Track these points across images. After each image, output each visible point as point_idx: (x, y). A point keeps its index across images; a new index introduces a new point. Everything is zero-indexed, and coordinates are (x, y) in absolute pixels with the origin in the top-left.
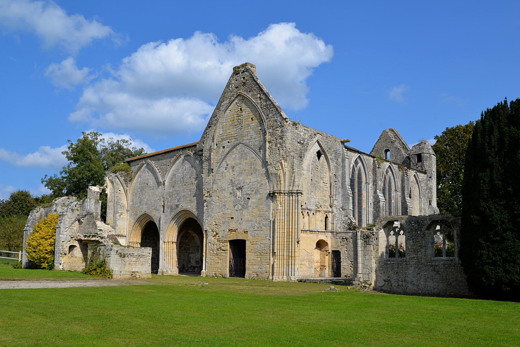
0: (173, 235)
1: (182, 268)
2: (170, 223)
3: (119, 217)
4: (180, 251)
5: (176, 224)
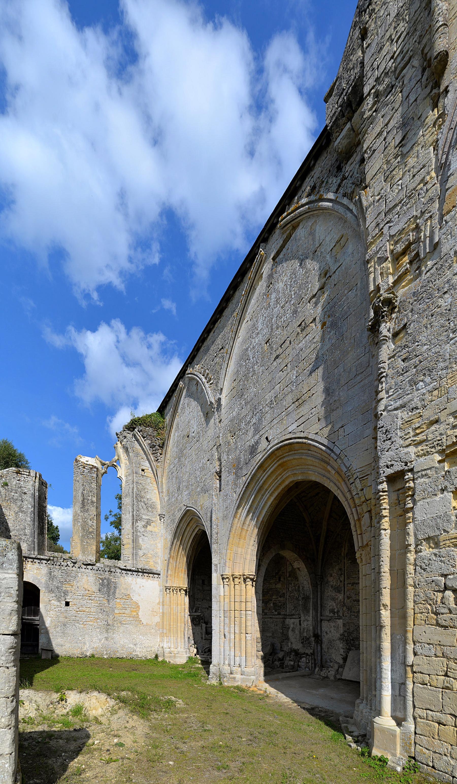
0: (246, 553)
1: (271, 655)
2: (235, 516)
3: (143, 529)
4: (266, 611)
5: (251, 519)
